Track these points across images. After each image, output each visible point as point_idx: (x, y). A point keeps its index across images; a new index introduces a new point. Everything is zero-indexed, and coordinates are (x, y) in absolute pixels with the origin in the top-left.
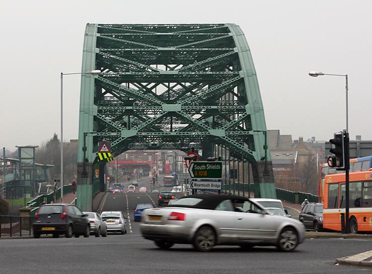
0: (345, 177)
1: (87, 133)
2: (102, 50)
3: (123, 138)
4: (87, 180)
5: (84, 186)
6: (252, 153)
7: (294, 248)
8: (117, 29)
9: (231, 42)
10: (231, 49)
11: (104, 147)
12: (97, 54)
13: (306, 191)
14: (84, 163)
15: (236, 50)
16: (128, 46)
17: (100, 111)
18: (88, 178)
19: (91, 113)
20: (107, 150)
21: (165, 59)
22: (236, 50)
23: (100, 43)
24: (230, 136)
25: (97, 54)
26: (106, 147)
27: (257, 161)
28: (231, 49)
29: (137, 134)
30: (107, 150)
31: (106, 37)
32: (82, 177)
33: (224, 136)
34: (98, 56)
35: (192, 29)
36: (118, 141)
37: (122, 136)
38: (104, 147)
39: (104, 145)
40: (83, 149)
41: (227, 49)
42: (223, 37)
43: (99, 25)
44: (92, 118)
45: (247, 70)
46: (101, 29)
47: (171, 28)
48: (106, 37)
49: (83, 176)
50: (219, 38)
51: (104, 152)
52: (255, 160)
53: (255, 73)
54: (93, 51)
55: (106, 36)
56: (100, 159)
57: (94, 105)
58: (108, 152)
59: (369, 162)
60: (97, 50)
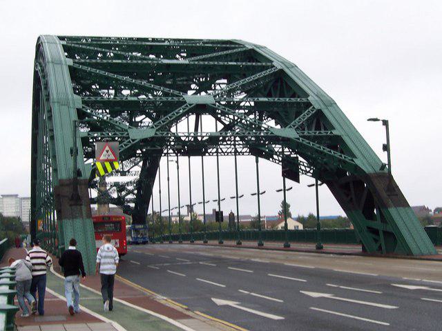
3: (133, 140)
4: (81, 209)
8: (101, 44)
11: (107, 151)
13: (430, 224)
14: (75, 179)
18: (83, 206)
20: (112, 157)
24: (304, 137)
26: (110, 152)
27: (367, 173)
29: (156, 134)
30: (112, 157)
32: (71, 205)
33: (298, 136)
36: (125, 145)
39: (107, 148)
40: (71, 151)
41: (206, 63)
46: (73, 46)
49: (72, 203)
51: (107, 160)
52: (365, 172)
54: (64, 63)
58: (115, 160)
59: (286, 179)
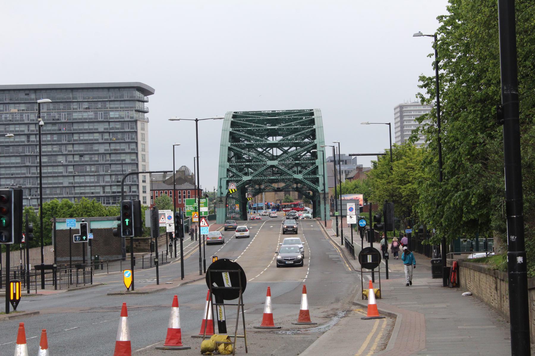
0: (242, 314)
1: (222, 178)
2: (233, 129)
5: (221, 209)
6: (317, 187)
7: (368, 219)
8: (246, 115)
9: (313, 122)
10: (312, 126)
11: (163, 218)
12: (230, 132)
15: (314, 127)
16: (251, 126)
17: (230, 166)
19: (225, 167)
21: (274, 133)
22: (314, 127)
23: (233, 124)
25: (230, 132)
28: (312, 126)
31: (237, 121)
34: (231, 133)
35: (88, 172)
37: (243, 180)
38: (163, 218)
42: (309, 119)
43: (234, 112)
44: (226, 170)
45: (319, 139)
47: (278, 114)
48: (237, 121)
50: (289, 124)
53: (324, 141)
55: (237, 120)
56: (230, 193)
57: (227, 163)
60: (231, 130)
